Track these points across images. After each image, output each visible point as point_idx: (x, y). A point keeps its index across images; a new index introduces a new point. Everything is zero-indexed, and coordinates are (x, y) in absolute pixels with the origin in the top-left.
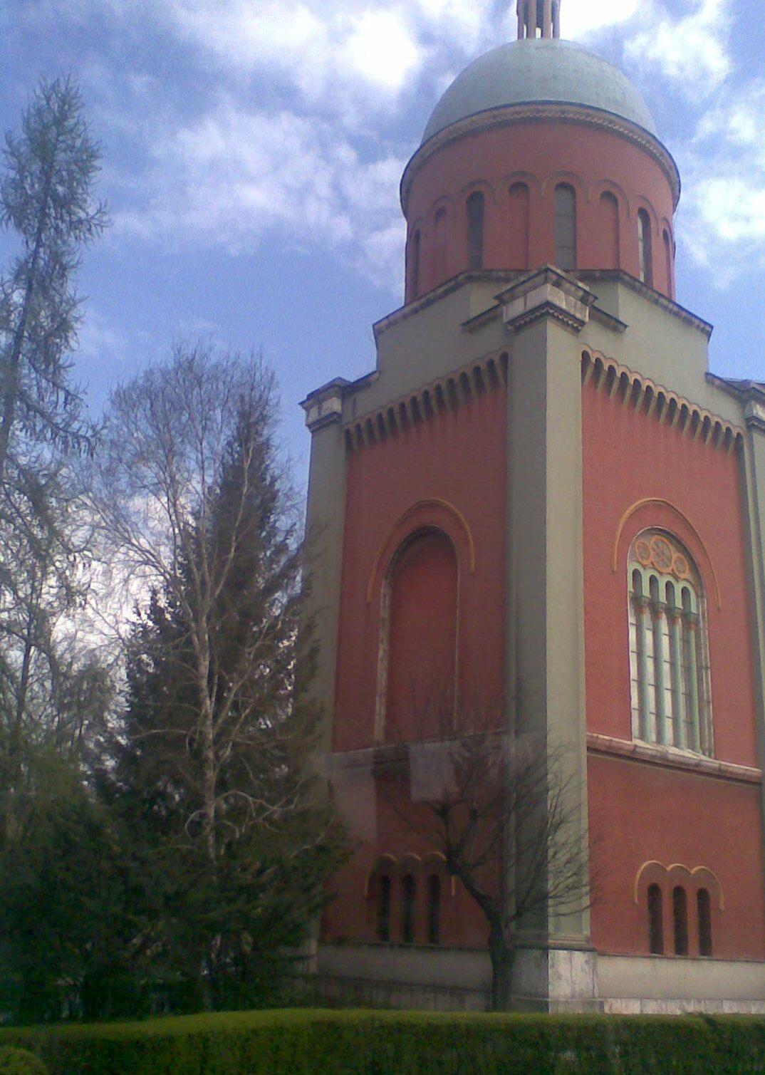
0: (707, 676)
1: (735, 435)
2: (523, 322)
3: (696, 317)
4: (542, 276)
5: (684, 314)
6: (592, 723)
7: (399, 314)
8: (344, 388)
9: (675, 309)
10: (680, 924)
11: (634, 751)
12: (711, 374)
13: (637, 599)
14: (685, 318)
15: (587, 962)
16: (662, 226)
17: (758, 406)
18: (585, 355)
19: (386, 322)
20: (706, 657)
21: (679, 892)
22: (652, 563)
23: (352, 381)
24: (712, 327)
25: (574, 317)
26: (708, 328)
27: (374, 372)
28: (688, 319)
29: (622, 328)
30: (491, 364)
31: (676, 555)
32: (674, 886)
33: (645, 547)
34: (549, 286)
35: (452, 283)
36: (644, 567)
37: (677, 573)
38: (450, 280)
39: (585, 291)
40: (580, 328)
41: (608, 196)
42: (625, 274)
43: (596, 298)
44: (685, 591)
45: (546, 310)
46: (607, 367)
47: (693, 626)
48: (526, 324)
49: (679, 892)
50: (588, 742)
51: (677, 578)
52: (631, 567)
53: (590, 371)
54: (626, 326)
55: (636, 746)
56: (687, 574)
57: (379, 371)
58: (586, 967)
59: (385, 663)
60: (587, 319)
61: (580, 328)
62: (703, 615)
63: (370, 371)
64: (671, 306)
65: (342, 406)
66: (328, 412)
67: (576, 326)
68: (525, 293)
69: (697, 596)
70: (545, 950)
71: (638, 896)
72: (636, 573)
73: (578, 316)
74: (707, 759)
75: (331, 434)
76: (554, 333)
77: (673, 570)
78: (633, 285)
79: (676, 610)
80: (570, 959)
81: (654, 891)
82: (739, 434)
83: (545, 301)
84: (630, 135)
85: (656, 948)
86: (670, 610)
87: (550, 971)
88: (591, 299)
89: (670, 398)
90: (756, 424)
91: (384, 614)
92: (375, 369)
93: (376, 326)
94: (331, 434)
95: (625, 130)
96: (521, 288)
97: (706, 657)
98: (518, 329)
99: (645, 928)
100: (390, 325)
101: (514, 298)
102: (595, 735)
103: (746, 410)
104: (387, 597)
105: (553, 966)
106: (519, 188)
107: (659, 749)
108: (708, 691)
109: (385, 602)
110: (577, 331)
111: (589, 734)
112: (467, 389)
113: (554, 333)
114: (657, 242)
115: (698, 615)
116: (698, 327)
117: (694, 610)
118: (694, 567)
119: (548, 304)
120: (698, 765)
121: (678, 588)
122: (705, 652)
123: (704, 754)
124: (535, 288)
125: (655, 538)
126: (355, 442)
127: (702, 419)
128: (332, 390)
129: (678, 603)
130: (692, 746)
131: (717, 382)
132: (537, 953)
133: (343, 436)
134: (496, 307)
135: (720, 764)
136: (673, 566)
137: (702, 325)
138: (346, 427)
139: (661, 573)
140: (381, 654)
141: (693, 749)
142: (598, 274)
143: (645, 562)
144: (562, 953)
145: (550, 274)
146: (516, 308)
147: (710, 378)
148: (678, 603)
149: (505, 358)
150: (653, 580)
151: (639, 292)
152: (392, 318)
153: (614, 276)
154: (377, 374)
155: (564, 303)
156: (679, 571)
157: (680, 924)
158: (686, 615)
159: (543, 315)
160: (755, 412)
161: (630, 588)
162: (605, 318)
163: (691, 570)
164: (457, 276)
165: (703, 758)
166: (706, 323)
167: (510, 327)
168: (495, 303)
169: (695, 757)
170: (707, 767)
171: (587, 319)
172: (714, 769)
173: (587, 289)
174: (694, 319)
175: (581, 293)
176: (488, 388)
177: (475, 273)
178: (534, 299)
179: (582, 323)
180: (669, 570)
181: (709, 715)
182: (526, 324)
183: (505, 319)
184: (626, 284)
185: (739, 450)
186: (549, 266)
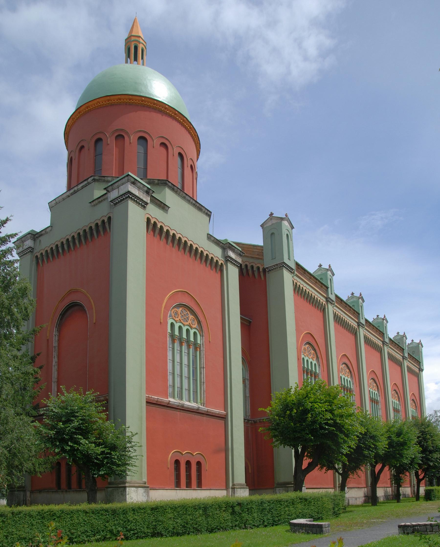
0: (204, 371)
1: (220, 264)
2: (117, 201)
3: (204, 207)
4: (126, 178)
5: (198, 205)
6: (149, 389)
7: (61, 198)
8: (34, 235)
9: (194, 202)
10: (189, 477)
11: (169, 403)
12: (210, 235)
13: (172, 335)
14: (198, 207)
15: (144, 492)
16: (190, 163)
17: (231, 252)
18: (148, 220)
19: (54, 202)
20: (203, 363)
21: (188, 463)
22: (180, 320)
23: (38, 232)
24: (211, 212)
25: (142, 200)
26: (209, 213)
27: (49, 226)
28: (200, 208)
29: (167, 208)
30: (103, 221)
31: (191, 317)
32: (186, 460)
33: (176, 313)
34: (129, 183)
35: (86, 182)
36: (176, 321)
37: (191, 325)
38: (85, 180)
39: (148, 188)
40: (145, 206)
41: (163, 145)
42: (169, 182)
43: (153, 192)
44: (195, 333)
45: (129, 195)
46: (153, 222)
47: (198, 349)
48: (119, 202)
49: (188, 463)
50: (146, 399)
51: (191, 328)
52: (170, 321)
53: (151, 227)
54: (169, 207)
55: (170, 401)
56: (196, 326)
57: (51, 226)
58: (145, 494)
59: (56, 367)
60: (149, 202)
61: (145, 206)
62: (203, 344)
63: (48, 226)
64: (192, 200)
65: (34, 244)
66: (27, 247)
67: (144, 205)
68: (118, 187)
69: (200, 335)
70: (125, 487)
71: (171, 466)
72: (172, 325)
73: (144, 199)
74: (203, 407)
75: (28, 257)
76: (132, 206)
77: (190, 324)
78: (173, 188)
79: (191, 342)
80: (137, 491)
81: (177, 462)
82: (222, 264)
83: (127, 191)
84: (183, 122)
85: (178, 485)
86: (188, 341)
87: (127, 496)
88: (151, 192)
89: (190, 244)
90: (229, 259)
91: (55, 344)
92: (49, 225)
93: (49, 204)
94: (28, 257)
95: (192, 132)
96: (116, 184)
97: (203, 363)
98: (115, 204)
99: (173, 478)
100: (57, 203)
101: (113, 190)
102: (150, 396)
103: (226, 253)
104: (56, 336)
105: (128, 494)
106: (120, 137)
107: (180, 402)
108: (204, 378)
109: (55, 339)
110: (145, 207)
111: (147, 396)
112: (92, 234)
113: (132, 206)
114: (187, 170)
115: (200, 344)
116: (204, 212)
117: (199, 342)
118: (199, 322)
119: (129, 192)
120: (198, 409)
121: (192, 332)
122: (204, 360)
123: (201, 405)
124: (123, 184)
125: (181, 309)
126: (40, 261)
127: (205, 255)
128: (29, 236)
129: (192, 339)
130: (196, 401)
131: (213, 239)
132: (122, 489)
133: (34, 259)
134: (106, 194)
135: (208, 409)
136: (189, 322)
137: (206, 211)
138: (36, 255)
139: (184, 325)
140: (54, 363)
141: (197, 403)
142: (156, 181)
143: (177, 319)
144: (133, 489)
145: (130, 177)
146: (114, 195)
147: (210, 237)
148: (192, 339)
149: (109, 218)
150: (180, 328)
151: (176, 192)
152: (57, 200)
153: (164, 183)
154: (50, 228)
155: (137, 193)
156: (193, 324)
157: (189, 477)
158: (195, 344)
159: (126, 198)
160: (229, 254)
161: (169, 330)
162: (159, 202)
163: (198, 324)
164: (88, 179)
165: (200, 406)
166: (208, 210)
167: (112, 204)
168: (105, 192)
169: (197, 406)
170: (202, 410)
171: (149, 202)
172: (205, 411)
173: (149, 187)
174: (203, 208)
175: (146, 189)
176: (102, 233)
177: (97, 178)
178: (122, 190)
179: (147, 204)
180: (188, 323)
181: (204, 389)
182: (119, 202)
183: (109, 200)
184: (170, 187)
185: (221, 271)
186: (130, 174)
